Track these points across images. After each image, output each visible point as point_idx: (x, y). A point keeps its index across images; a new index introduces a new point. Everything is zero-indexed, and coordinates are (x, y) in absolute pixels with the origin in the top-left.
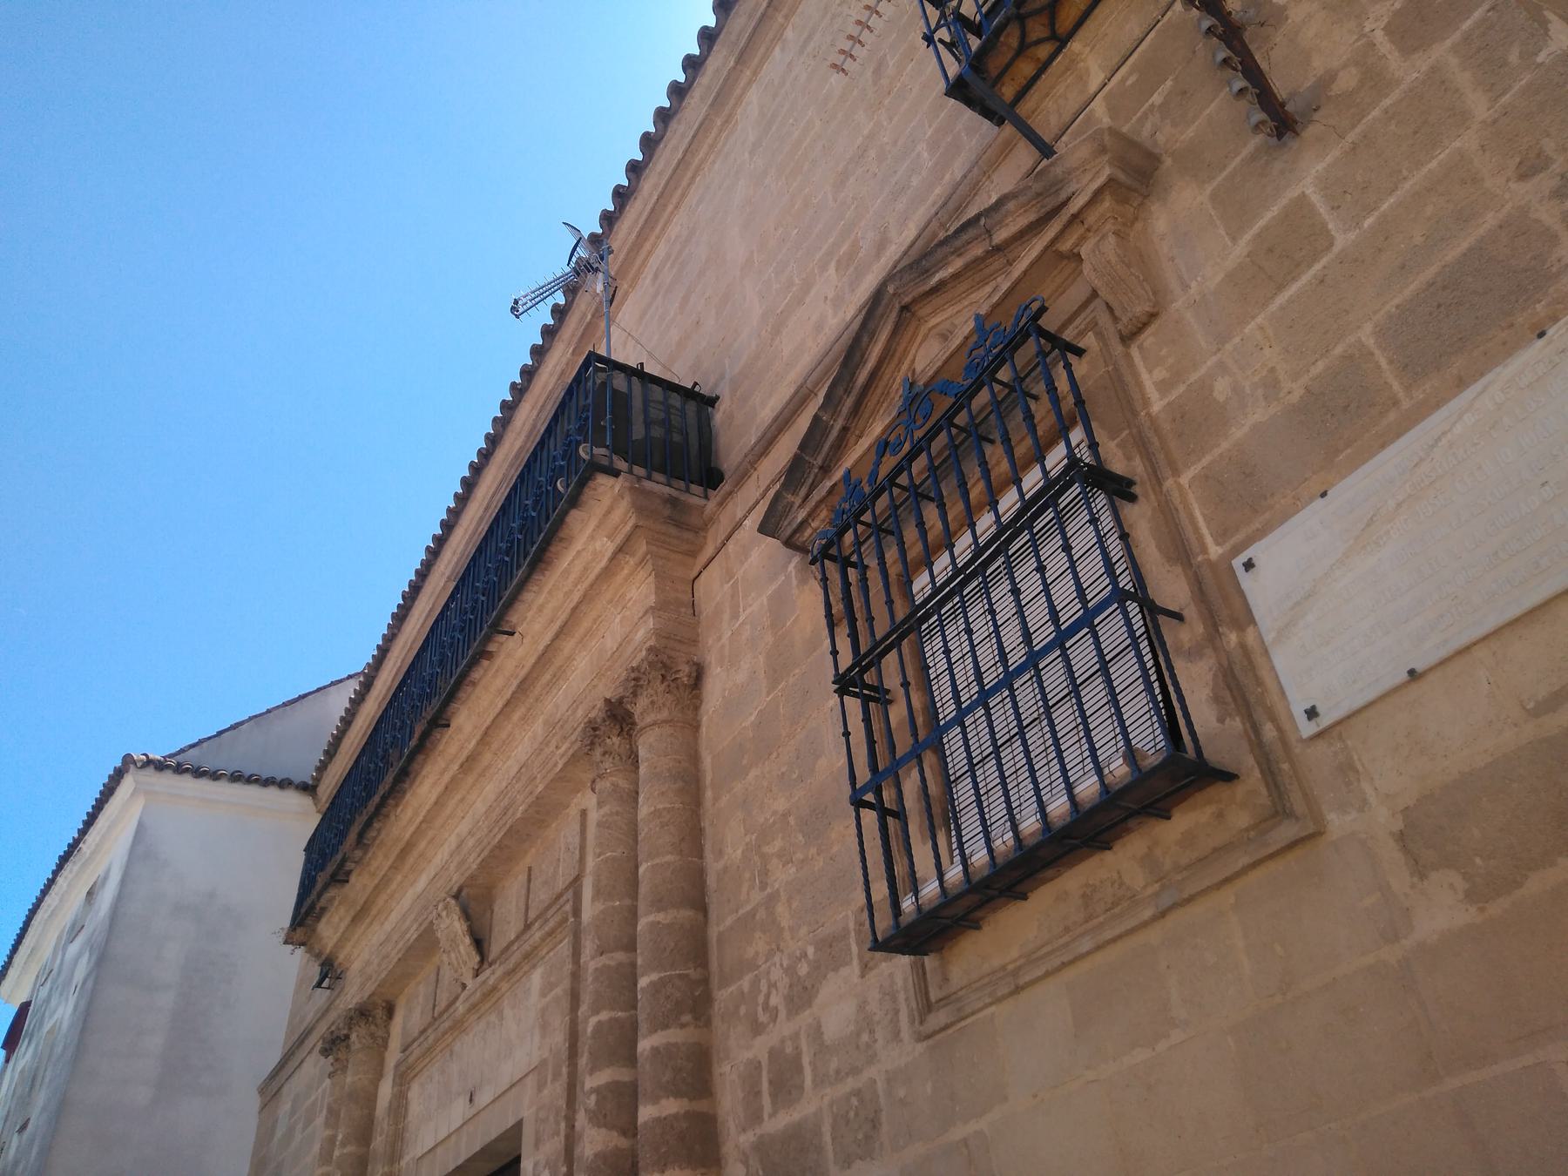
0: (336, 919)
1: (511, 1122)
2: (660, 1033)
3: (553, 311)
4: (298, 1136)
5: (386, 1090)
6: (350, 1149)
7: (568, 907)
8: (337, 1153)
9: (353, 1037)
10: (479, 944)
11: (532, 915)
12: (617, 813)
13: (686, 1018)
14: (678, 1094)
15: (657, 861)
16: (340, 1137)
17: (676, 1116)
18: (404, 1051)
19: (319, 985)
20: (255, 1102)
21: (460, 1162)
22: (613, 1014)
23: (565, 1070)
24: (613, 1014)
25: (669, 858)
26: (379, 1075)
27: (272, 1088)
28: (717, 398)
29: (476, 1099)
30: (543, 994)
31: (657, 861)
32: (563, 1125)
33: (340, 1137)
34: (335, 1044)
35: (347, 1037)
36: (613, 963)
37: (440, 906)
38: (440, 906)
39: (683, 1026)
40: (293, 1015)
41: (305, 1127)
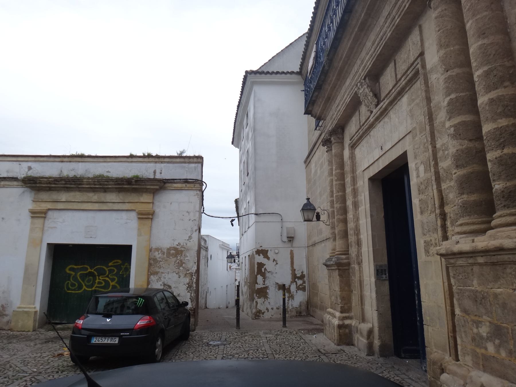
0: (319, 103)
1: (401, 153)
2: (493, 92)
3: (186, 302)
4: (319, 172)
5: (347, 153)
6: (338, 171)
7: (419, 66)
8: (334, 173)
9: (332, 139)
10: (376, 95)
11: (399, 76)
12: (445, 10)
13: (507, 83)
14: (507, 116)
15: (478, 16)
16: (334, 168)
17: (507, 126)
18: (350, 140)
19: (316, 129)
20: (304, 166)
21: (380, 169)
22: (457, 94)
23: (428, 128)
24: (457, 94)
25: (485, 13)
26: (343, 149)
27: (307, 161)
28: (305, 114)
29: (383, 148)
30: (409, 104)
31: (478, 16)
32: (430, 147)
33: (334, 168)
34: (327, 142)
35: (330, 139)
36: (454, 74)
37: (359, 84)
38: (359, 84)
39: (505, 87)
40: (309, 141)
41: (320, 169)
